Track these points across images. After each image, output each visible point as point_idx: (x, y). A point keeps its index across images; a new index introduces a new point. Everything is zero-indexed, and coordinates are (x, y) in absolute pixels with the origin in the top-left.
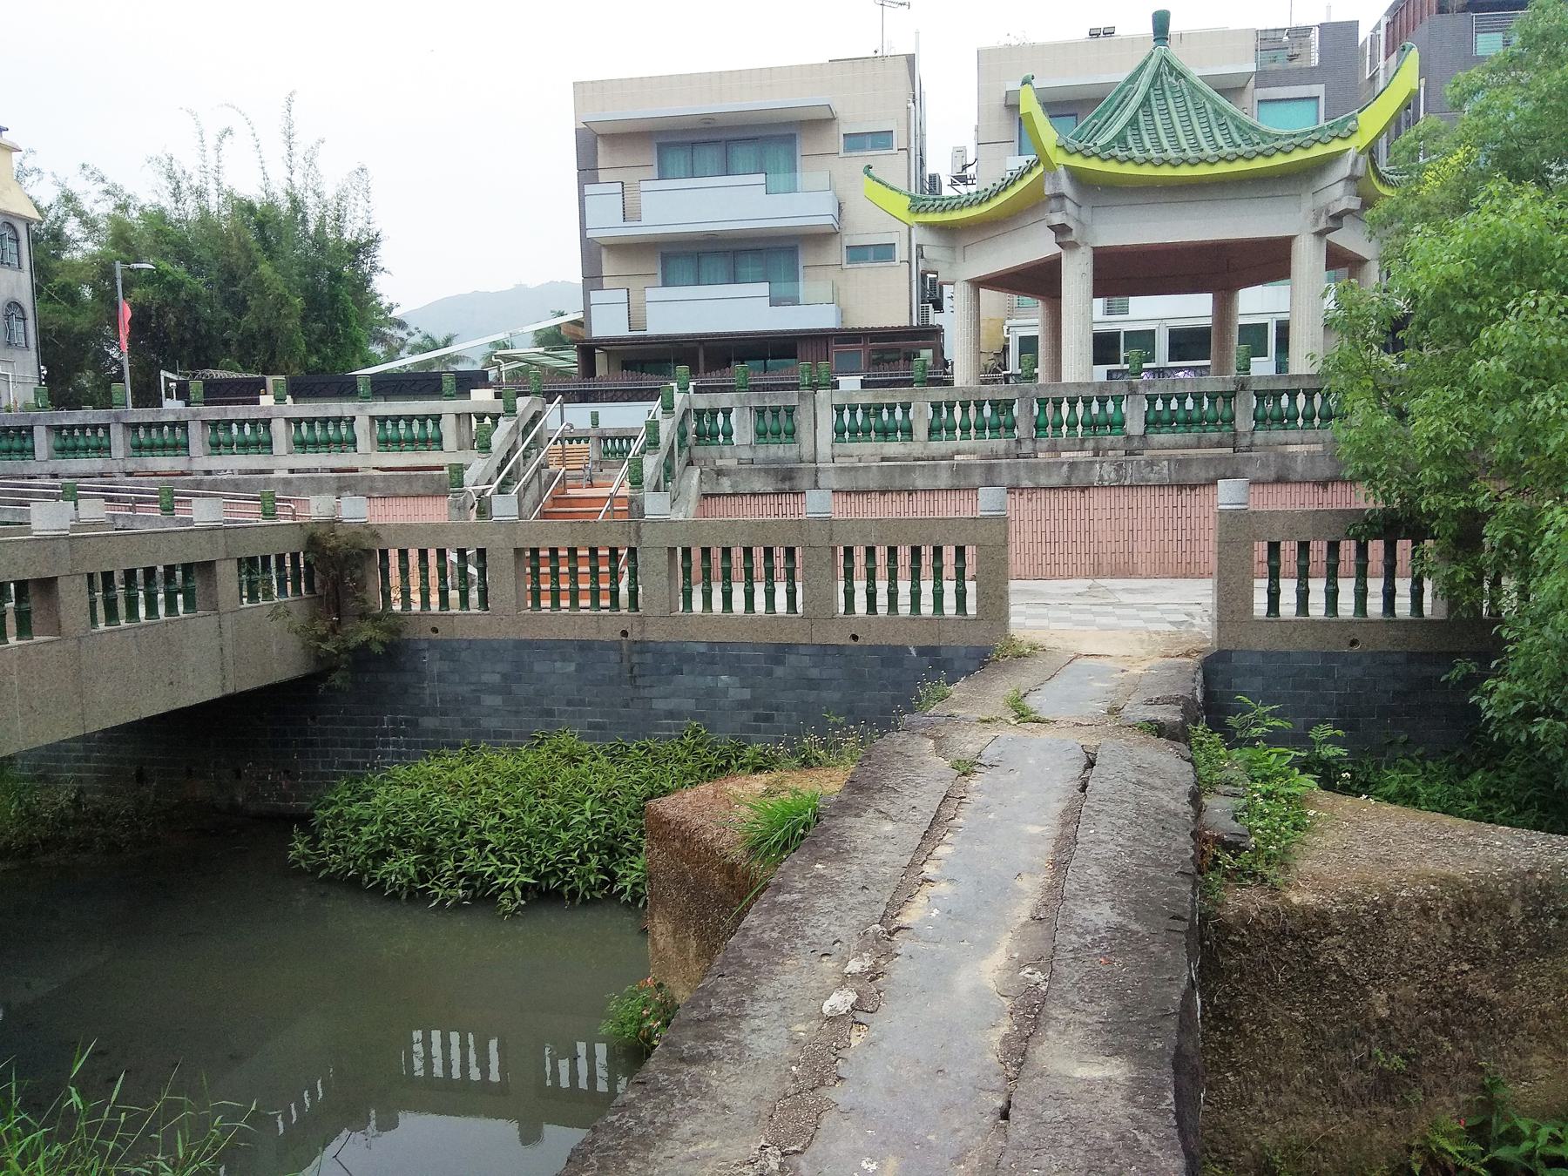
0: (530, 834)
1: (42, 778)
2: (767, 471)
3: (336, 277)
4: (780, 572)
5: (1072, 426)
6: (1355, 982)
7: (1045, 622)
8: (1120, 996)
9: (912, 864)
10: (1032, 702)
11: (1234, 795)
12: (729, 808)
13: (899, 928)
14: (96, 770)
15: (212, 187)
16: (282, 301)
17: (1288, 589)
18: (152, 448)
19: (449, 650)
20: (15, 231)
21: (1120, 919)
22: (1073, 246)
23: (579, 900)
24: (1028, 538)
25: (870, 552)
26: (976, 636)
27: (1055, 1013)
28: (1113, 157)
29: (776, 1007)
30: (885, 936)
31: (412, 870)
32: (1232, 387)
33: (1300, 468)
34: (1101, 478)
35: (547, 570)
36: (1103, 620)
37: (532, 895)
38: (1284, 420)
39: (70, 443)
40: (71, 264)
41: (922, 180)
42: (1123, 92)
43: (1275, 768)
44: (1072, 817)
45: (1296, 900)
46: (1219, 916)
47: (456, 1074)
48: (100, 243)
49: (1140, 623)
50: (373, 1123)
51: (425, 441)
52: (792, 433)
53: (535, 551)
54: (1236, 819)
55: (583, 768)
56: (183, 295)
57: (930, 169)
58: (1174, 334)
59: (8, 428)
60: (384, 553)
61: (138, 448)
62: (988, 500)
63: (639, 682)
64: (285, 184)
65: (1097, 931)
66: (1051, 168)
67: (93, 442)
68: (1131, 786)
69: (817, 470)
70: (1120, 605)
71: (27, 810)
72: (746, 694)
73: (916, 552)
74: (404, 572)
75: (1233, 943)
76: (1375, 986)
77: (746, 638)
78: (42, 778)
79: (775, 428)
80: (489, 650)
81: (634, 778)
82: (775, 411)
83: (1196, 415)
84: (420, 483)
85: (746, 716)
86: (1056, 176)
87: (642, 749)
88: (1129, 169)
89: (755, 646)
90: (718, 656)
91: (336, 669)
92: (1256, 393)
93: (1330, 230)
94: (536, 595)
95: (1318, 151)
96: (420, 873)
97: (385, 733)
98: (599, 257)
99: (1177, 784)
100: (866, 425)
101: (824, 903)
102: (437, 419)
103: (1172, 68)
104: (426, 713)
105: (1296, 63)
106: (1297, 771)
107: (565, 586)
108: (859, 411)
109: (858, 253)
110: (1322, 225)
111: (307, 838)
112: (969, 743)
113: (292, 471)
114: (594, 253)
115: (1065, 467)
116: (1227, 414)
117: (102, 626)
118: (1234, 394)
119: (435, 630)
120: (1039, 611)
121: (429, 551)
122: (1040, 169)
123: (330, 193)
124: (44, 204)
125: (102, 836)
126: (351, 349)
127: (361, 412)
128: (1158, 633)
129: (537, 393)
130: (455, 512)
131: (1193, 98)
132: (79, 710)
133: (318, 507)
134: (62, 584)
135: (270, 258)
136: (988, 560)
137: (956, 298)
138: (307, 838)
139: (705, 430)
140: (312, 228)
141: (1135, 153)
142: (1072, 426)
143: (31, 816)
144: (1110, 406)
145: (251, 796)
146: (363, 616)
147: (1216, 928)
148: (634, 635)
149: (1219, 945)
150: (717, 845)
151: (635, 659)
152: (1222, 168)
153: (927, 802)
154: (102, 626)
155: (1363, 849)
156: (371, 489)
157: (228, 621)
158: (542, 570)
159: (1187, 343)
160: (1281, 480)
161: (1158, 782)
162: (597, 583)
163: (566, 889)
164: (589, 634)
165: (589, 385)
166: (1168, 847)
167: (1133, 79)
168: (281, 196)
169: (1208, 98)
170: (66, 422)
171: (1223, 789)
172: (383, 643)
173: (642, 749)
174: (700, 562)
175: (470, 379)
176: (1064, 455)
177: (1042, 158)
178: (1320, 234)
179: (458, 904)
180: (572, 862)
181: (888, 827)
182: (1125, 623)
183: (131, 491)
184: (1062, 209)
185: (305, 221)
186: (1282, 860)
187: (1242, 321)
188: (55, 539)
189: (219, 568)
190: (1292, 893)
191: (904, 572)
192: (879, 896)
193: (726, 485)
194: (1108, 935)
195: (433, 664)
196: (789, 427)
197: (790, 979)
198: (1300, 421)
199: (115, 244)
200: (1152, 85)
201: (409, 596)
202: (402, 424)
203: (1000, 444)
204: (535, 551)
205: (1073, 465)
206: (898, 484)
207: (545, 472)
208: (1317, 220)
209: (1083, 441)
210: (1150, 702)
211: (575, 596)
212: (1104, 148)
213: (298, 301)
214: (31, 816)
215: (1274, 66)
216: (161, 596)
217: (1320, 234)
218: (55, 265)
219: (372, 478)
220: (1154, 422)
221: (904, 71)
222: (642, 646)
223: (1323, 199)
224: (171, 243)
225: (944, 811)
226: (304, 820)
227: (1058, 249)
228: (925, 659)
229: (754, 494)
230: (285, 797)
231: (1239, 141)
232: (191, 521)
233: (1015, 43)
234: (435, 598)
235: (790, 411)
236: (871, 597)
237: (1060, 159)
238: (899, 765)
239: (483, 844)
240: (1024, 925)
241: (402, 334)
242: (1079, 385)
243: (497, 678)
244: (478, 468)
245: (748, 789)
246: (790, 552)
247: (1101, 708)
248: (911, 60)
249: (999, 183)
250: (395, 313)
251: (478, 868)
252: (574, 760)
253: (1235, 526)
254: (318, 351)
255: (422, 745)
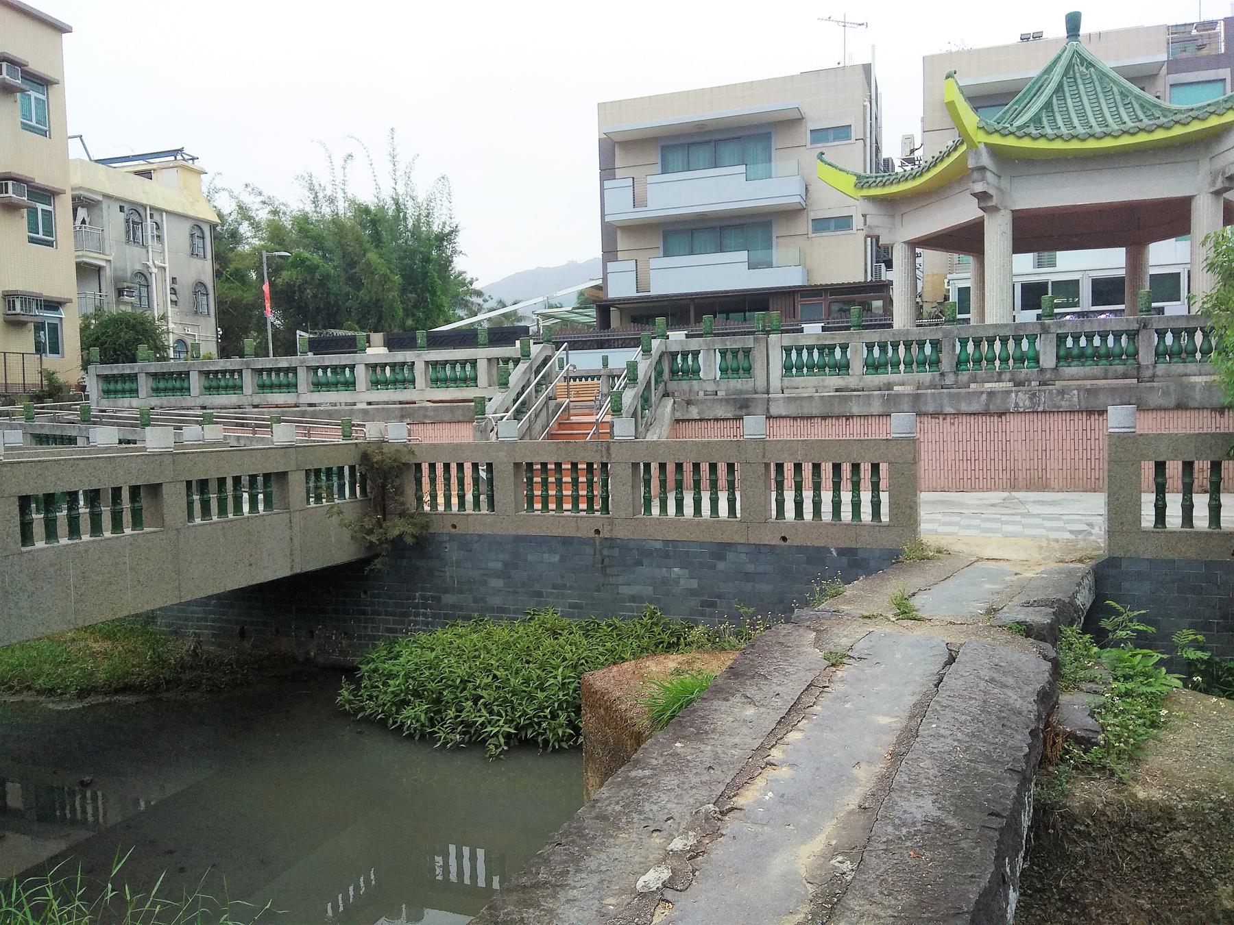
0: (514, 693)
1: (175, 632)
2: (727, 401)
3: (427, 260)
4: (705, 483)
5: (1004, 360)
6: (1201, 874)
7: (955, 529)
8: (919, 890)
9: (761, 747)
10: (916, 602)
11: (1095, 692)
12: (639, 681)
13: (732, 809)
14: (213, 628)
15: (340, 195)
16: (385, 279)
17: (1174, 503)
18: (272, 387)
19: (464, 542)
20: (202, 232)
21: (939, 813)
22: (994, 210)
23: (550, 749)
24: (951, 456)
25: (798, 467)
26: (888, 541)
27: (852, 903)
28: (1027, 135)
29: (595, 879)
30: (714, 820)
31: (423, 717)
32: (1135, 326)
33: (1198, 397)
34: (1017, 405)
35: (539, 480)
36: (1010, 528)
37: (513, 742)
38: (1182, 354)
39: (214, 383)
40: (242, 256)
41: (877, 164)
42: (1038, 85)
43: (1139, 668)
44: (920, 711)
45: (1141, 795)
46: (1065, 806)
47: (467, 881)
48: (261, 239)
49: (1043, 532)
50: (404, 915)
51: (465, 380)
52: (748, 370)
53: (530, 465)
54: (1092, 715)
55: (561, 640)
56: (317, 276)
57: (885, 155)
58: (1096, 283)
59: (172, 373)
60: (418, 466)
61: (262, 387)
62: (900, 424)
63: (608, 571)
64: (392, 192)
65: (914, 824)
66: (973, 146)
67: (231, 383)
68: (983, 684)
69: (769, 400)
70: (1028, 515)
71: (158, 657)
72: (694, 584)
73: (837, 468)
74: (433, 480)
75: (1079, 832)
76: (1220, 879)
77: (693, 537)
78: (175, 632)
79: (735, 365)
80: (494, 543)
81: (601, 649)
82: (735, 353)
83: (1103, 351)
84: (460, 412)
85: (694, 602)
86: (977, 153)
87: (609, 626)
88: (1042, 144)
89: (702, 544)
90: (671, 552)
91: (377, 556)
92: (1156, 331)
93: (1226, 190)
94: (530, 500)
95: (1214, 121)
96: (431, 720)
97: (416, 606)
98: (614, 236)
99: (1028, 682)
100: (821, 363)
101: (670, 780)
102: (474, 363)
103: (1083, 60)
104: (446, 591)
105: (1204, 52)
106: (1164, 670)
107: (583, 493)
108: (816, 351)
109: (821, 225)
110: (1219, 185)
111: (352, 687)
112: (842, 637)
113: (369, 404)
114: (612, 234)
115: (984, 396)
116: (1131, 349)
117: (198, 521)
118: (1137, 332)
119: (454, 526)
120: (941, 520)
121: (452, 468)
122: (964, 147)
123: (421, 197)
124: (225, 211)
125: (208, 679)
126: (436, 312)
127: (419, 358)
128: (1057, 541)
129: (548, 341)
130: (478, 434)
131: (1101, 83)
132: (176, 584)
133: (372, 431)
134: (165, 489)
135: (377, 246)
136: (900, 473)
137: (899, 256)
138: (352, 687)
139: (676, 369)
140: (410, 223)
141: (1049, 131)
142: (1004, 360)
143: (159, 661)
144: (1025, 344)
145: (293, 655)
146: (402, 514)
147: (1062, 816)
148: (605, 533)
149: (1065, 833)
150: (629, 714)
151: (606, 552)
152: (1126, 140)
153: (788, 688)
154: (198, 521)
155: (1217, 749)
156: (425, 417)
157: (297, 518)
158: (535, 479)
159: (1107, 290)
160: (1181, 406)
161: (1010, 681)
162: (547, 490)
163: (540, 739)
164: (570, 532)
165: (604, 335)
166: (1004, 745)
167: (1049, 70)
168: (390, 202)
169: (1114, 82)
170: (212, 368)
171: (1084, 686)
172: (414, 536)
173: (609, 626)
174: (677, 475)
175: (515, 333)
176: (987, 385)
177: (964, 138)
178: (1217, 193)
179: (457, 748)
180: (545, 717)
181: (750, 712)
182: (1028, 531)
183: (256, 419)
184: (983, 179)
185: (405, 218)
186: (1134, 756)
187: (1153, 271)
188: (161, 454)
189: (291, 477)
190: (1138, 787)
191: (846, 485)
192: (722, 777)
193: (694, 412)
194: (923, 829)
195: (453, 553)
196: (746, 365)
197: (617, 852)
198: (1198, 356)
199: (271, 239)
200: (1066, 74)
201: (439, 501)
202: (458, 367)
203: (926, 376)
204: (530, 465)
205: (991, 394)
206: (837, 410)
207: (552, 403)
208: (1214, 182)
209: (1000, 374)
210: (1028, 604)
211: (560, 500)
212: (1019, 128)
213: (397, 278)
214: (159, 661)
215: (1184, 55)
216: (261, 496)
217: (1217, 193)
218: (231, 255)
219: (426, 409)
220: (1064, 358)
221: (861, 77)
222: (611, 542)
223: (1219, 163)
224: (312, 237)
225: (804, 699)
226: (351, 672)
227: (980, 213)
228: (845, 560)
229: (717, 420)
230: (343, 653)
231: (1141, 116)
232: (145, 449)
233: (954, 49)
234: (455, 501)
235: (747, 352)
236: (799, 505)
237: (981, 138)
238: (777, 655)
239: (476, 699)
240: (851, 813)
241: (479, 300)
242: (996, 326)
243: (499, 565)
244: (498, 399)
245: (662, 667)
246: (731, 467)
247: (979, 608)
248: (867, 69)
249: (931, 160)
250: (476, 286)
251: (472, 718)
252: (555, 633)
253: (1125, 448)
254: (413, 315)
255: (448, 617)
